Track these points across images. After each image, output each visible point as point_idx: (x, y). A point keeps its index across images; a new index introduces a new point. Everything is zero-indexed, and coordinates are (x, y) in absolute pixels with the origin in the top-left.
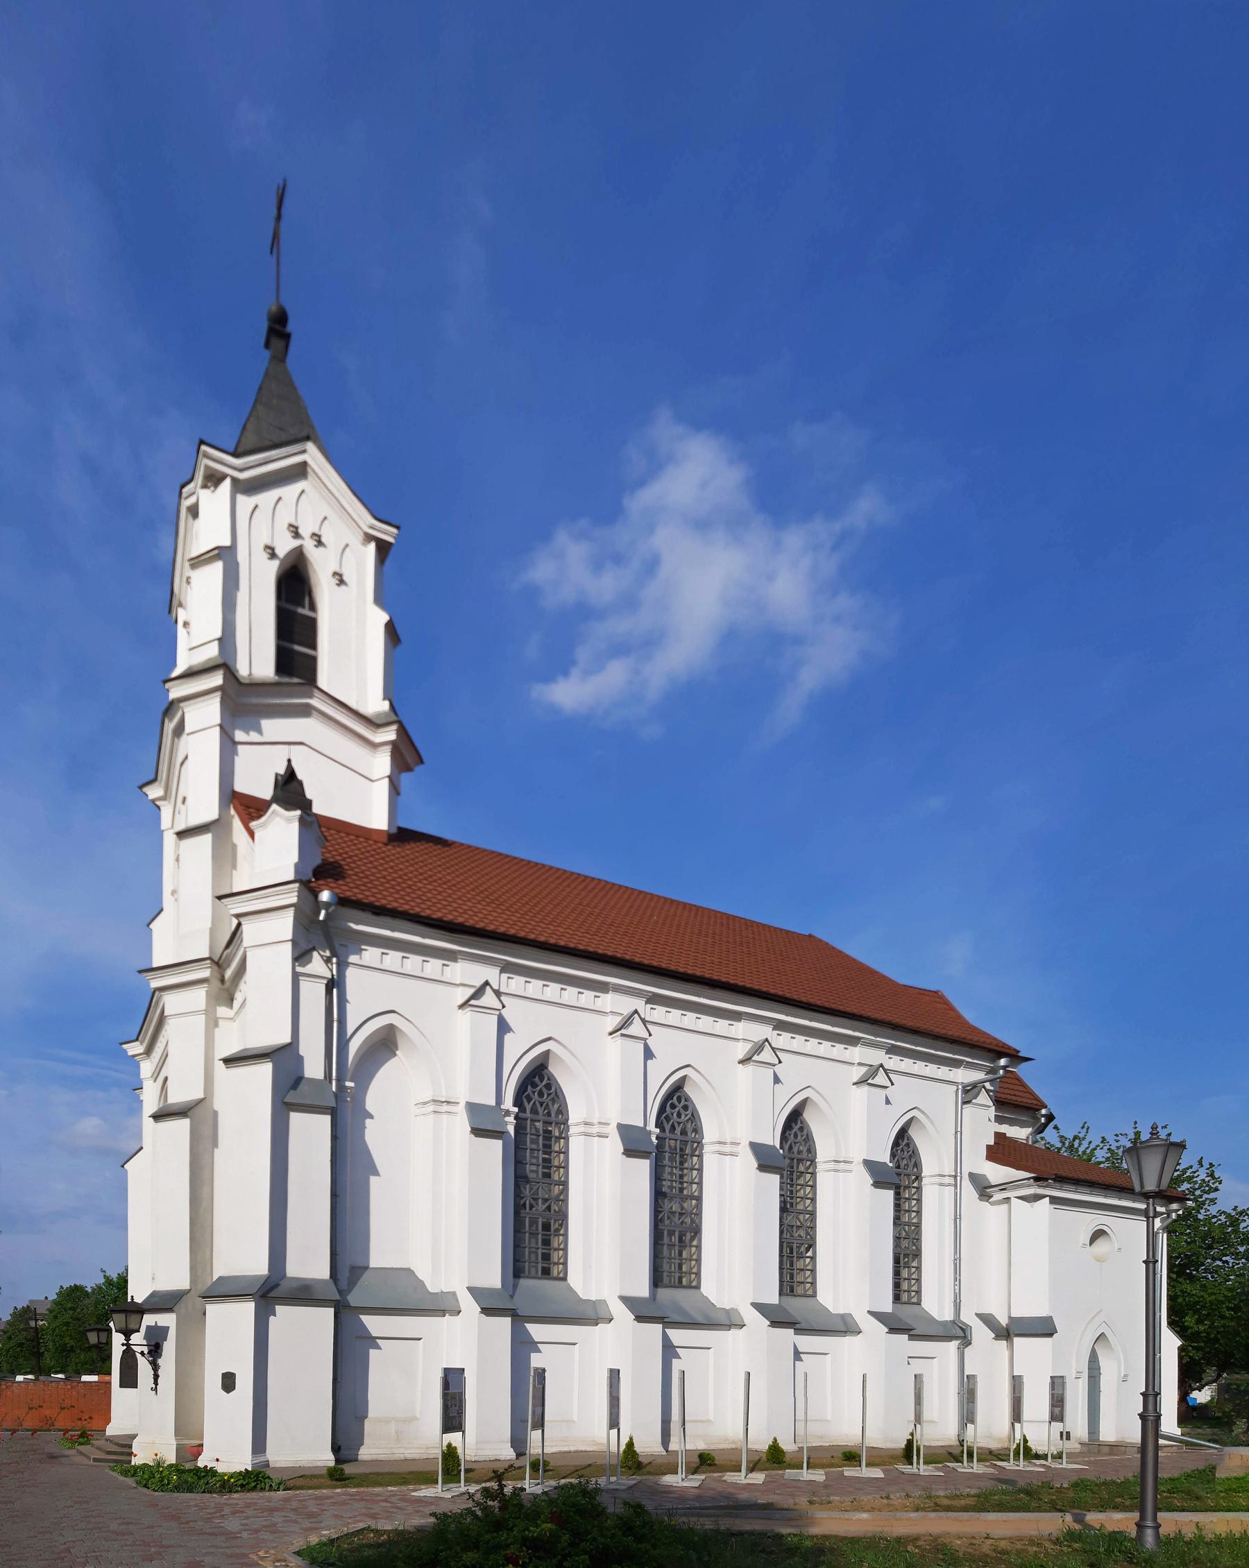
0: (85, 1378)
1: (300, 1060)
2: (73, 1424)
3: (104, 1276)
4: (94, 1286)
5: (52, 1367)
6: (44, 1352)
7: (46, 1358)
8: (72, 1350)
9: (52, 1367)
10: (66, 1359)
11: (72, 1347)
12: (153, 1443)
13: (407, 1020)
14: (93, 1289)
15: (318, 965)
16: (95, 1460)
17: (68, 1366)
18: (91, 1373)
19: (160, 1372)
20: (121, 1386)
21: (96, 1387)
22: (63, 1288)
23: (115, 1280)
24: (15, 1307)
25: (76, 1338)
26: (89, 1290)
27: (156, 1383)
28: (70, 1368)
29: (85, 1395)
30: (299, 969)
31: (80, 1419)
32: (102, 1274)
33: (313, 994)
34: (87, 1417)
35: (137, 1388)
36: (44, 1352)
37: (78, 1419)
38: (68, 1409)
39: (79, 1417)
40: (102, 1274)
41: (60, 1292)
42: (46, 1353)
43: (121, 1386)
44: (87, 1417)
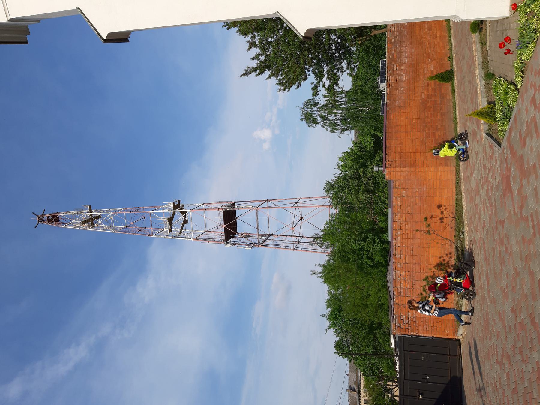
2: (448, 229)
13: (257, 218)
22: (336, 352)
24: (334, 353)
26: (338, 338)
31: (441, 219)
32: (328, 331)
34: (438, 211)
37: (442, 222)
39: (439, 221)
40: (328, 331)
41: (339, 354)
44: (438, 211)
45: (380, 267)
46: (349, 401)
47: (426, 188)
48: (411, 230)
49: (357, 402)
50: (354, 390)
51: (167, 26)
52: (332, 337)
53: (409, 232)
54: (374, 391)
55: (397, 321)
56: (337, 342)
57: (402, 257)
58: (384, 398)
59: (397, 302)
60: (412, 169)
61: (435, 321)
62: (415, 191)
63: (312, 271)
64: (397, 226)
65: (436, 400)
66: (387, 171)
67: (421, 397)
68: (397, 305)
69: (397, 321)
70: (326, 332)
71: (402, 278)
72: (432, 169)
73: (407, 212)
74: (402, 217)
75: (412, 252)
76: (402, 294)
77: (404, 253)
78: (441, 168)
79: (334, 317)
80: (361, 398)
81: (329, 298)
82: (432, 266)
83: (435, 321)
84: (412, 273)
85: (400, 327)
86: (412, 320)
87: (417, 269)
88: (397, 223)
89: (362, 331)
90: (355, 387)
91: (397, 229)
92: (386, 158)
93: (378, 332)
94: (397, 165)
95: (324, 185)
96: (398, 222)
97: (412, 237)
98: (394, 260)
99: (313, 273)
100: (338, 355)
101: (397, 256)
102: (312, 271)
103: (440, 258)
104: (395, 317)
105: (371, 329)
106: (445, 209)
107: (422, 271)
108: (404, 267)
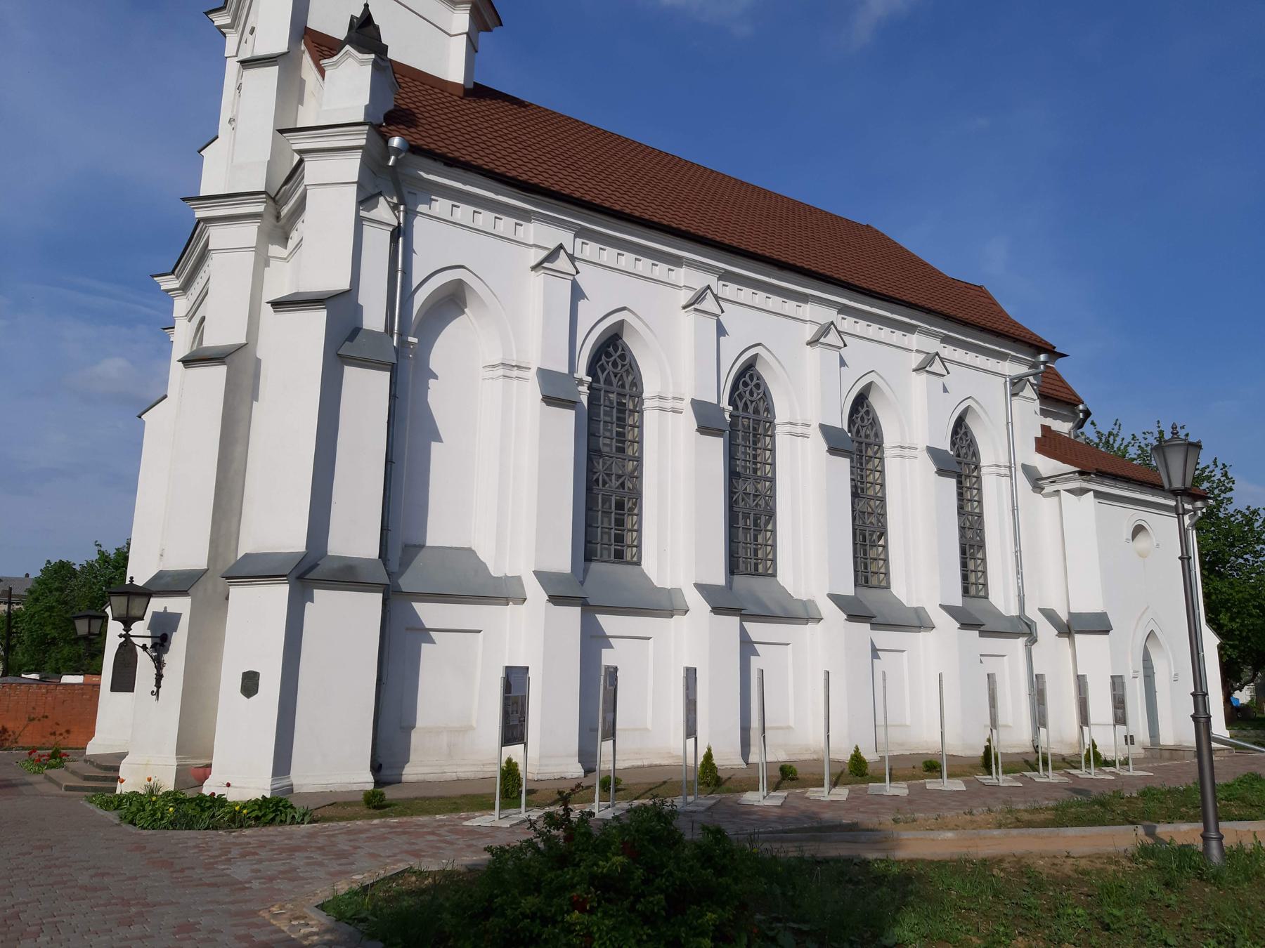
0: (67, 679)
1: (358, 310)
2: (44, 740)
4: (85, 563)
5: (24, 665)
6: (15, 645)
7: (17, 653)
8: (54, 642)
9: (24, 665)
10: (44, 653)
11: (54, 639)
15: (383, 211)
17: (46, 662)
19: (164, 671)
20: (113, 689)
21: (80, 691)
23: (112, 556)
25: (61, 627)
26: (78, 568)
27: (158, 685)
30: (363, 213)
31: (54, 734)
33: (377, 242)
34: (63, 731)
36: (15, 645)
37: (51, 734)
38: (39, 720)
39: (53, 731)
41: (46, 568)
43: (113, 689)
51: (251, 295)
74: (61, 693)
79: (119, 564)
91: (48, 688)
95: (1091, 411)
103: (13, 732)
106: (64, 738)
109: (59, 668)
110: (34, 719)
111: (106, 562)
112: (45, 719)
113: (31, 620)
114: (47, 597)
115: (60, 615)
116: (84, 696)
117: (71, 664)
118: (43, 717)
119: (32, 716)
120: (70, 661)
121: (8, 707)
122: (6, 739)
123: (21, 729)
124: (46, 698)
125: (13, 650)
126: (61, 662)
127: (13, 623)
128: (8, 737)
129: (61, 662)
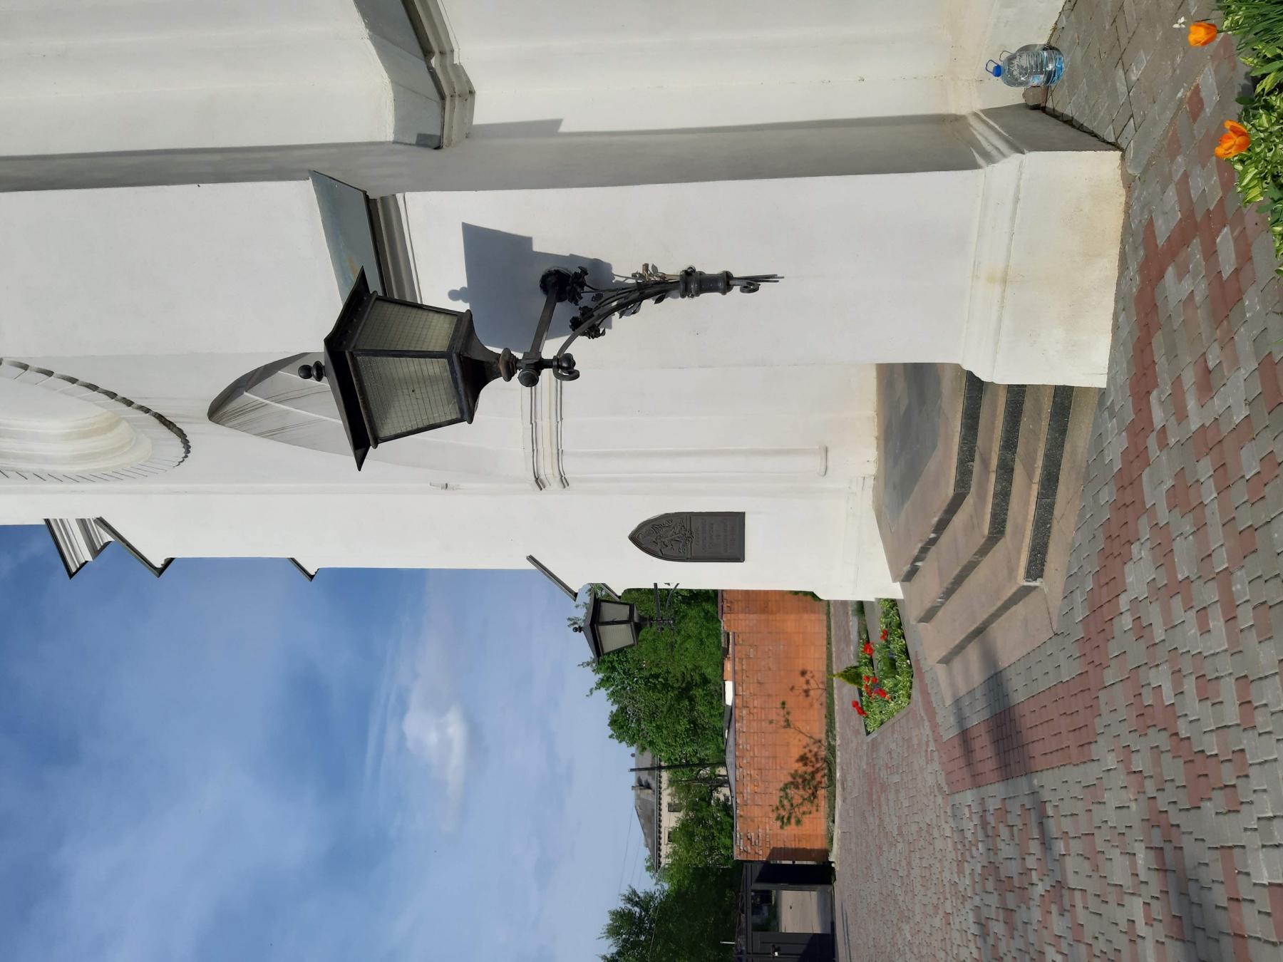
0: (729, 699)
2: (817, 705)
3: (596, 688)
4: (610, 702)
5: (718, 747)
6: (698, 758)
7: (706, 755)
8: (693, 722)
9: (718, 747)
10: (705, 729)
11: (690, 722)
12: (1004, 281)
14: (615, 702)
16: (1036, 568)
17: (714, 726)
18: (722, 695)
19: (672, 268)
20: (738, 557)
21: (744, 662)
23: (601, 675)
25: (678, 716)
27: (724, 283)
28: (718, 725)
29: (759, 683)
31: (807, 692)
32: (595, 692)
34: (802, 680)
35: (743, 514)
36: (698, 758)
37: (807, 696)
38: (788, 713)
41: (618, 737)
42: (698, 755)
43: (738, 557)
45: (704, 604)
46: (637, 810)
47: (784, 645)
48: (762, 708)
49: (653, 811)
50: (648, 787)
52: (603, 706)
53: (760, 710)
54: (689, 790)
55: (742, 842)
56: (615, 714)
57: (748, 748)
58: (709, 804)
59: (742, 813)
60: (763, 617)
61: (797, 839)
62: (767, 650)
63: (569, 619)
64: (741, 703)
65: (799, 957)
66: (725, 619)
67: (776, 954)
68: (742, 819)
69: (742, 842)
70: (589, 693)
71: (749, 778)
72: (793, 617)
73: (755, 681)
75: (763, 740)
76: (749, 802)
77: (752, 743)
78: (806, 616)
79: (609, 667)
80: (662, 802)
81: (648, 884)
82: (794, 759)
83: (797, 839)
84: (763, 771)
85: (747, 852)
86: (764, 840)
87: (771, 764)
88: (741, 697)
89: (667, 693)
90: (650, 781)
92: (722, 596)
93: (698, 693)
94: (740, 609)
96: (743, 696)
97: (763, 718)
98: (737, 753)
99: (572, 622)
100: (618, 739)
101: (741, 747)
102: (569, 619)
103: (805, 747)
104: (738, 836)
105: (685, 692)
107: (778, 767)
108: (752, 763)
109: (720, 714)
110: (787, 721)
111: (607, 680)
112: (786, 706)
113: (673, 746)
114: (647, 733)
115: (665, 718)
116: (752, 656)
117: (715, 703)
118: (784, 708)
119: (783, 724)
120: (712, 703)
121: (769, 757)
122: (816, 755)
123: (801, 736)
124: (755, 707)
125: (704, 760)
126: (713, 712)
127: (677, 763)
128: (813, 753)
129: (713, 712)
